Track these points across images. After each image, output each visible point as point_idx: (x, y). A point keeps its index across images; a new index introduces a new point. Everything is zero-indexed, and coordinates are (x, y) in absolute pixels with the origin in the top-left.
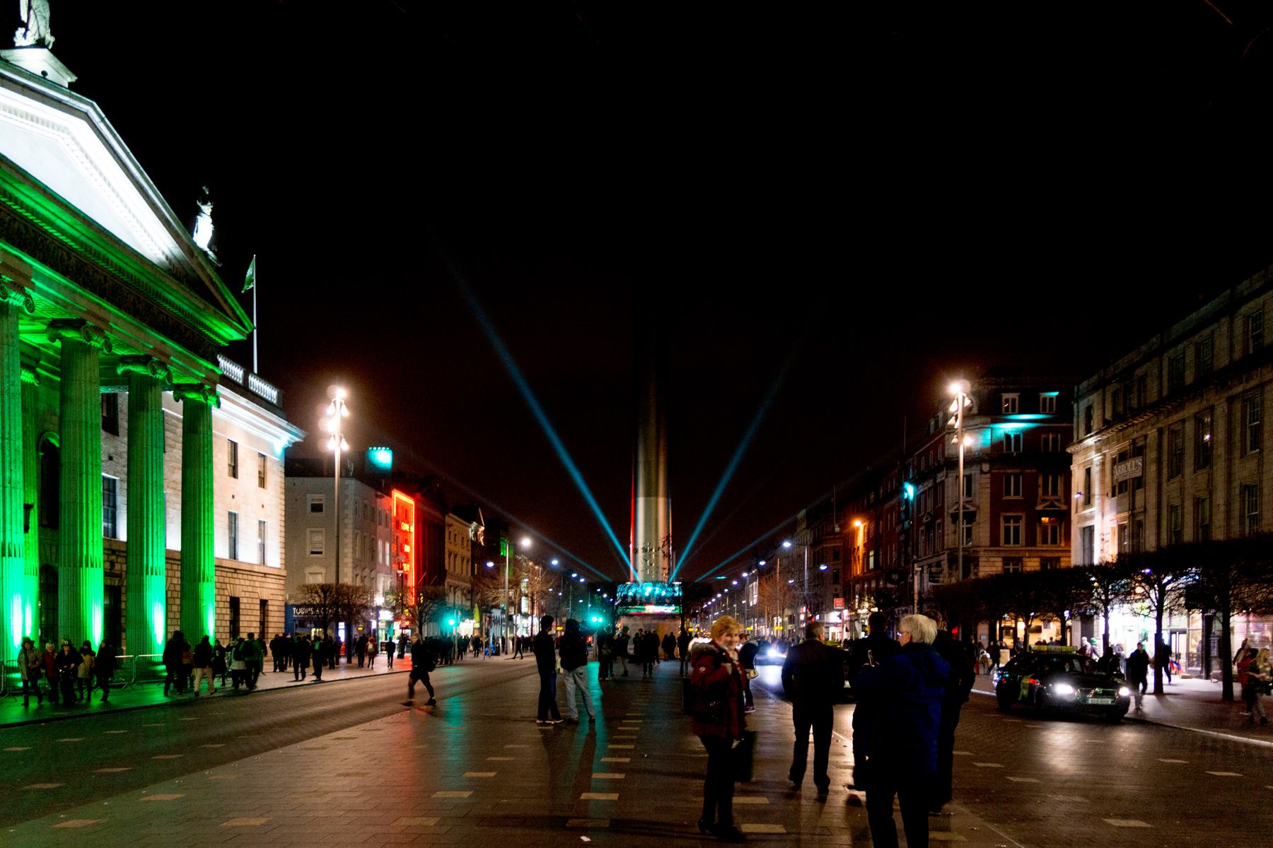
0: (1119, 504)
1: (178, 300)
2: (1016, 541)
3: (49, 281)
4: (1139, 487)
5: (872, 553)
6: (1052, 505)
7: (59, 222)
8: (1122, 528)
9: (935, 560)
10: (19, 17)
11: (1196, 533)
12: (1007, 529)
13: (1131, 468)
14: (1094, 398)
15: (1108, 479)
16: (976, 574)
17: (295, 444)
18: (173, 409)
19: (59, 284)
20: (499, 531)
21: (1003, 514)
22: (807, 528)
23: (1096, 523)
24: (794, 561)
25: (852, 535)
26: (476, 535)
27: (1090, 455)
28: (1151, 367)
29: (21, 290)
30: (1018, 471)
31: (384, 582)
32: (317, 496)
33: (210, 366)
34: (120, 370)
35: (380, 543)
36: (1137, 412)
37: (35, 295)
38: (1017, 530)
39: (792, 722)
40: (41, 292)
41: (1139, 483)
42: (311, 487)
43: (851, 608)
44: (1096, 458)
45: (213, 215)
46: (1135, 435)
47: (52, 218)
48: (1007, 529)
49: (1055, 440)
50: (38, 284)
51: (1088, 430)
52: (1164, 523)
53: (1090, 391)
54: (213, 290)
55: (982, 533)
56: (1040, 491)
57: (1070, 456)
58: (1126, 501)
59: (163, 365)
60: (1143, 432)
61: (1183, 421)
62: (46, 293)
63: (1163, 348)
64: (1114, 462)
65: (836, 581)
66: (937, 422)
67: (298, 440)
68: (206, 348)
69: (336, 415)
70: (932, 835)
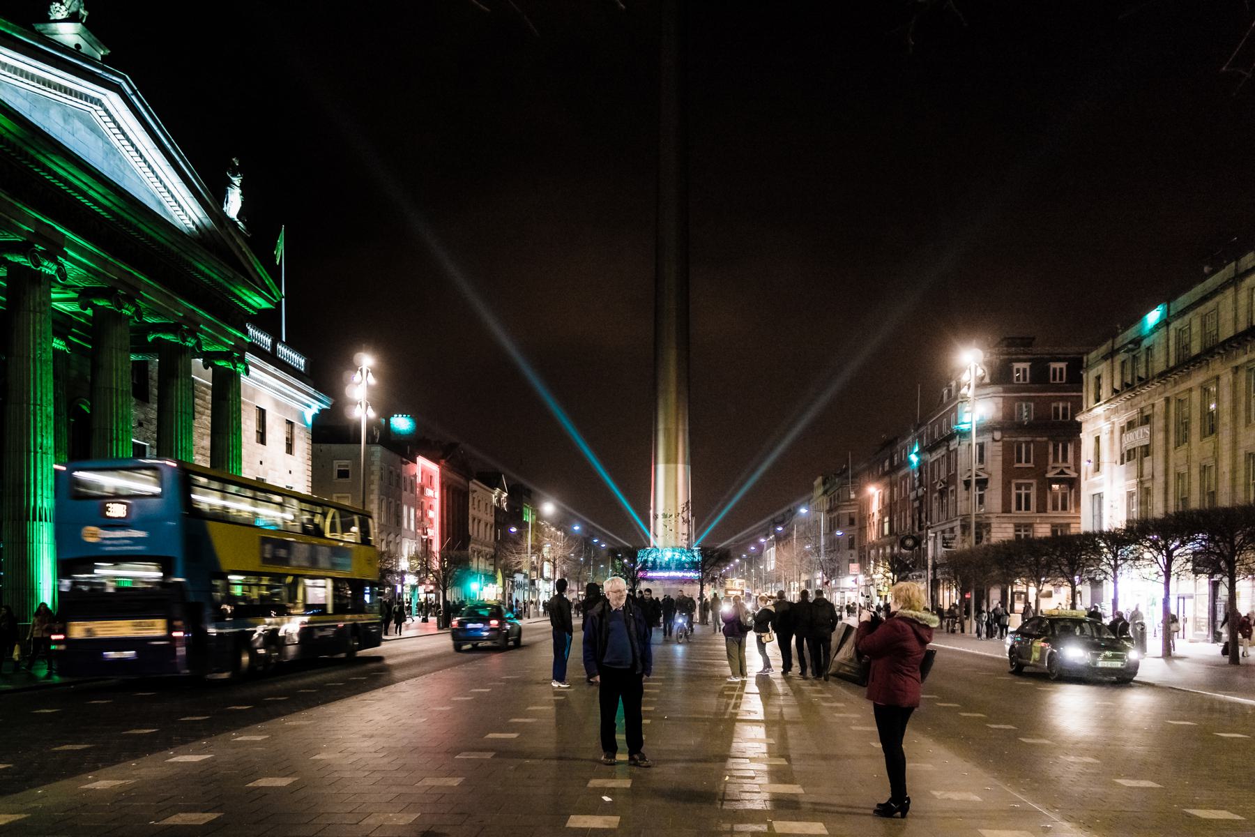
0: (1127, 472)
1: (207, 269)
2: (1027, 508)
4: (1147, 455)
5: (886, 519)
6: (1062, 472)
8: (1130, 495)
9: (948, 526)
13: (1138, 437)
14: (1103, 368)
16: (988, 540)
18: (202, 375)
20: (521, 496)
23: (1106, 490)
24: (810, 531)
25: (864, 505)
26: (499, 501)
27: (1101, 424)
30: (1029, 439)
34: (150, 338)
35: (405, 508)
36: (1144, 382)
37: (68, 265)
38: (1027, 496)
40: (72, 260)
41: (1146, 451)
43: (866, 573)
45: (241, 187)
46: (1143, 404)
47: (85, 188)
48: (1019, 496)
49: (1065, 409)
52: (1171, 490)
53: (1097, 363)
54: (241, 258)
55: (994, 498)
59: (192, 333)
60: (1151, 401)
61: (1190, 390)
64: (1122, 430)
65: (851, 547)
66: (950, 391)
67: (324, 407)
68: (239, 318)
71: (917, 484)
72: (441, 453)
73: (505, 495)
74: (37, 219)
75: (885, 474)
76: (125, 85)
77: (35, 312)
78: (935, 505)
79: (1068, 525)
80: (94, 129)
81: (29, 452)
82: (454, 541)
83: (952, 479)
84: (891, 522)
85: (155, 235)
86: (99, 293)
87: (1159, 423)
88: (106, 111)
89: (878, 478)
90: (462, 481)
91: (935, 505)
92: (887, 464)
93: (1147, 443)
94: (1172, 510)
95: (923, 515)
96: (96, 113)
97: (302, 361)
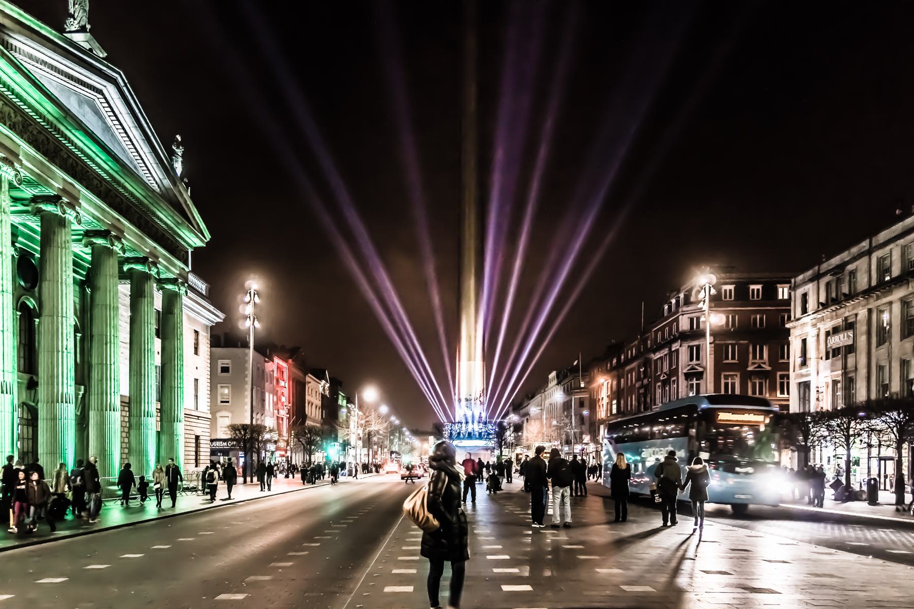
0: (833, 365)
1: (165, 217)
3: (90, 201)
5: (615, 402)
6: (760, 366)
7: (97, 159)
8: (835, 383)
10: (68, 10)
11: (902, 386)
12: (726, 385)
14: (810, 288)
21: (779, 373)
22: (558, 384)
26: (324, 390)
27: (808, 330)
28: (862, 263)
33: (182, 266)
34: (125, 268)
35: (267, 394)
36: (850, 297)
41: (851, 349)
44: (811, 334)
45: (182, 156)
46: (847, 314)
47: (93, 155)
49: (761, 319)
53: (805, 283)
56: (751, 356)
57: (789, 330)
58: (839, 364)
59: (155, 264)
60: (855, 312)
61: (891, 303)
62: (89, 210)
63: (869, 253)
64: (828, 334)
66: (670, 308)
67: (219, 320)
72: (288, 355)
73: (328, 385)
75: (613, 369)
76: (119, 79)
77: (62, 248)
80: (97, 112)
81: (58, 351)
83: (674, 372)
84: (618, 404)
86: (104, 234)
87: (862, 328)
88: (105, 98)
89: (608, 372)
91: (659, 391)
92: (615, 361)
93: (850, 342)
94: (873, 396)
95: (648, 400)
96: (99, 101)
97: (204, 287)
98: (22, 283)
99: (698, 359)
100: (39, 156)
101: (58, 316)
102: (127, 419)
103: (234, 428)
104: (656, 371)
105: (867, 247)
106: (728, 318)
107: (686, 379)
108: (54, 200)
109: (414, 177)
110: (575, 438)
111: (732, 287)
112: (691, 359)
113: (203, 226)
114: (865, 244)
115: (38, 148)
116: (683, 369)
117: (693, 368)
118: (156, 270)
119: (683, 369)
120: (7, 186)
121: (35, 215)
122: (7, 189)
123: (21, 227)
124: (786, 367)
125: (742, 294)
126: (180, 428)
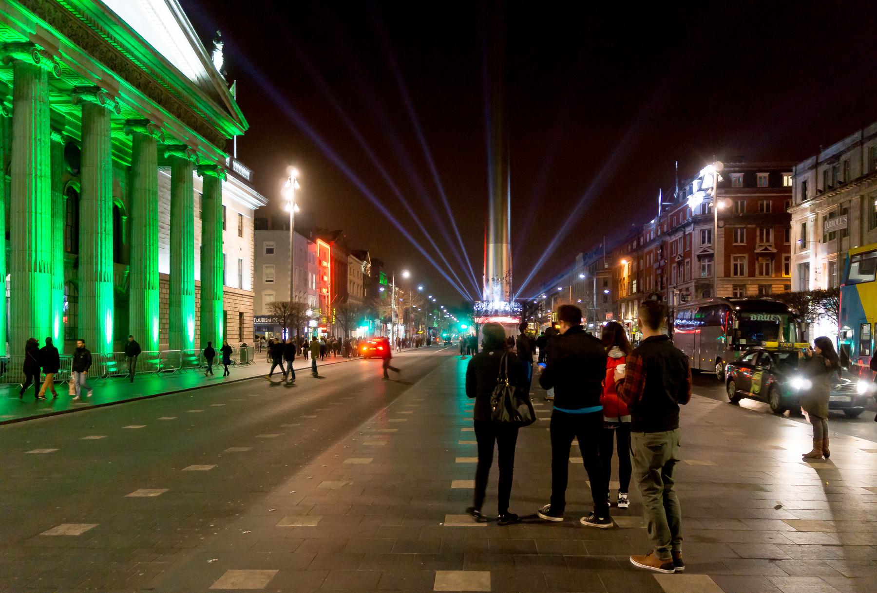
0: (829, 247)
1: (204, 108)
2: (742, 274)
3: (129, 93)
4: (845, 236)
5: (635, 282)
6: (766, 249)
8: (831, 264)
9: (685, 286)
12: (736, 266)
15: (820, 231)
17: (261, 207)
18: (198, 180)
19: (135, 94)
25: (621, 269)
26: (365, 270)
27: (805, 215)
29: (112, 98)
30: (742, 226)
31: (312, 301)
32: (272, 243)
34: (166, 155)
35: (310, 275)
36: (843, 184)
37: (121, 103)
39: (464, 386)
40: (123, 100)
41: (845, 233)
42: (271, 238)
44: (811, 216)
45: (224, 50)
46: (842, 200)
47: (132, 49)
48: (736, 266)
49: (768, 205)
50: (122, 94)
51: (804, 197)
53: (804, 171)
56: (758, 239)
58: (835, 246)
59: (194, 151)
60: (849, 198)
62: (126, 101)
63: (861, 143)
64: (825, 219)
69: (292, 189)
70: (570, 459)
71: (660, 258)
73: (370, 265)
74: (103, 71)
75: (633, 251)
77: (101, 136)
78: (674, 272)
79: (770, 286)
82: (339, 298)
83: (688, 254)
85: (173, 83)
86: (143, 123)
90: (344, 256)
91: (674, 272)
92: (635, 244)
93: (845, 227)
95: (665, 279)
98: (69, 169)
99: (709, 241)
100: (78, 49)
101: (97, 200)
102: (167, 296)
103: (275, 305)
104: (672, 253)
105: (860, 138)
106: (737, 203)
107: (699, 260)
108: (94, 90)
109: (75, 62)
110: (597, 316)
111: (741, 175)
112: (704, 242)
113: (241, 116)
114: (857, 136)
115: (77, 42)
116: (696, 251)
117: (705, 251)
118: (195, 157)
119: (696, 251)
120: (46, 76)
121: (76, 104)
122: (46, 79)
123: (68, 117)
124: (788, 249)
125: (750, 182)
126: (219, 307)
